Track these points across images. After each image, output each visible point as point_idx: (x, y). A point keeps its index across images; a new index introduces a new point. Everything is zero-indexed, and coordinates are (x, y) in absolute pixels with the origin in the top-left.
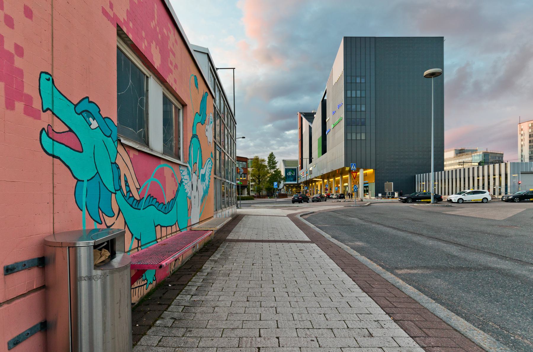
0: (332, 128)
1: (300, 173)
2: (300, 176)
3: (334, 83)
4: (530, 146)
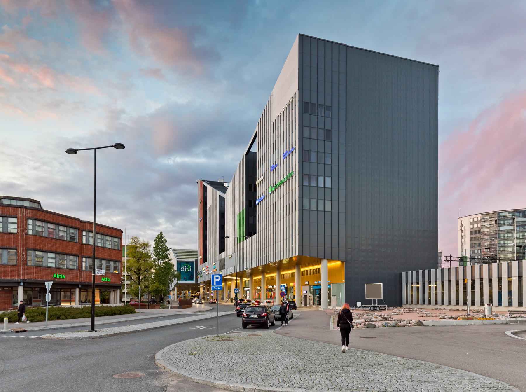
0: (270, 192)
1: (202, 268)
2: (200, 273)
3: (273, 121)
4: (471, 244)
